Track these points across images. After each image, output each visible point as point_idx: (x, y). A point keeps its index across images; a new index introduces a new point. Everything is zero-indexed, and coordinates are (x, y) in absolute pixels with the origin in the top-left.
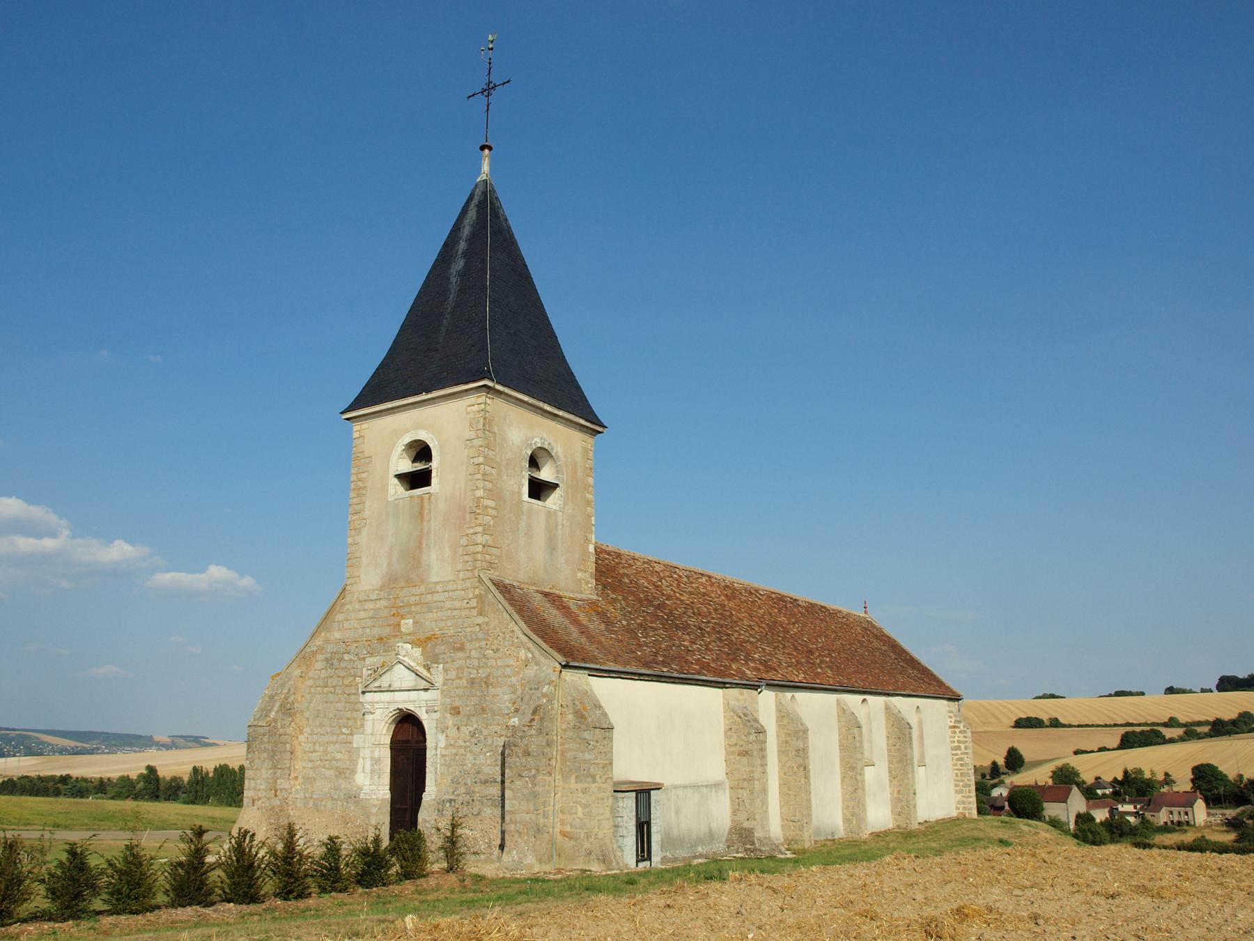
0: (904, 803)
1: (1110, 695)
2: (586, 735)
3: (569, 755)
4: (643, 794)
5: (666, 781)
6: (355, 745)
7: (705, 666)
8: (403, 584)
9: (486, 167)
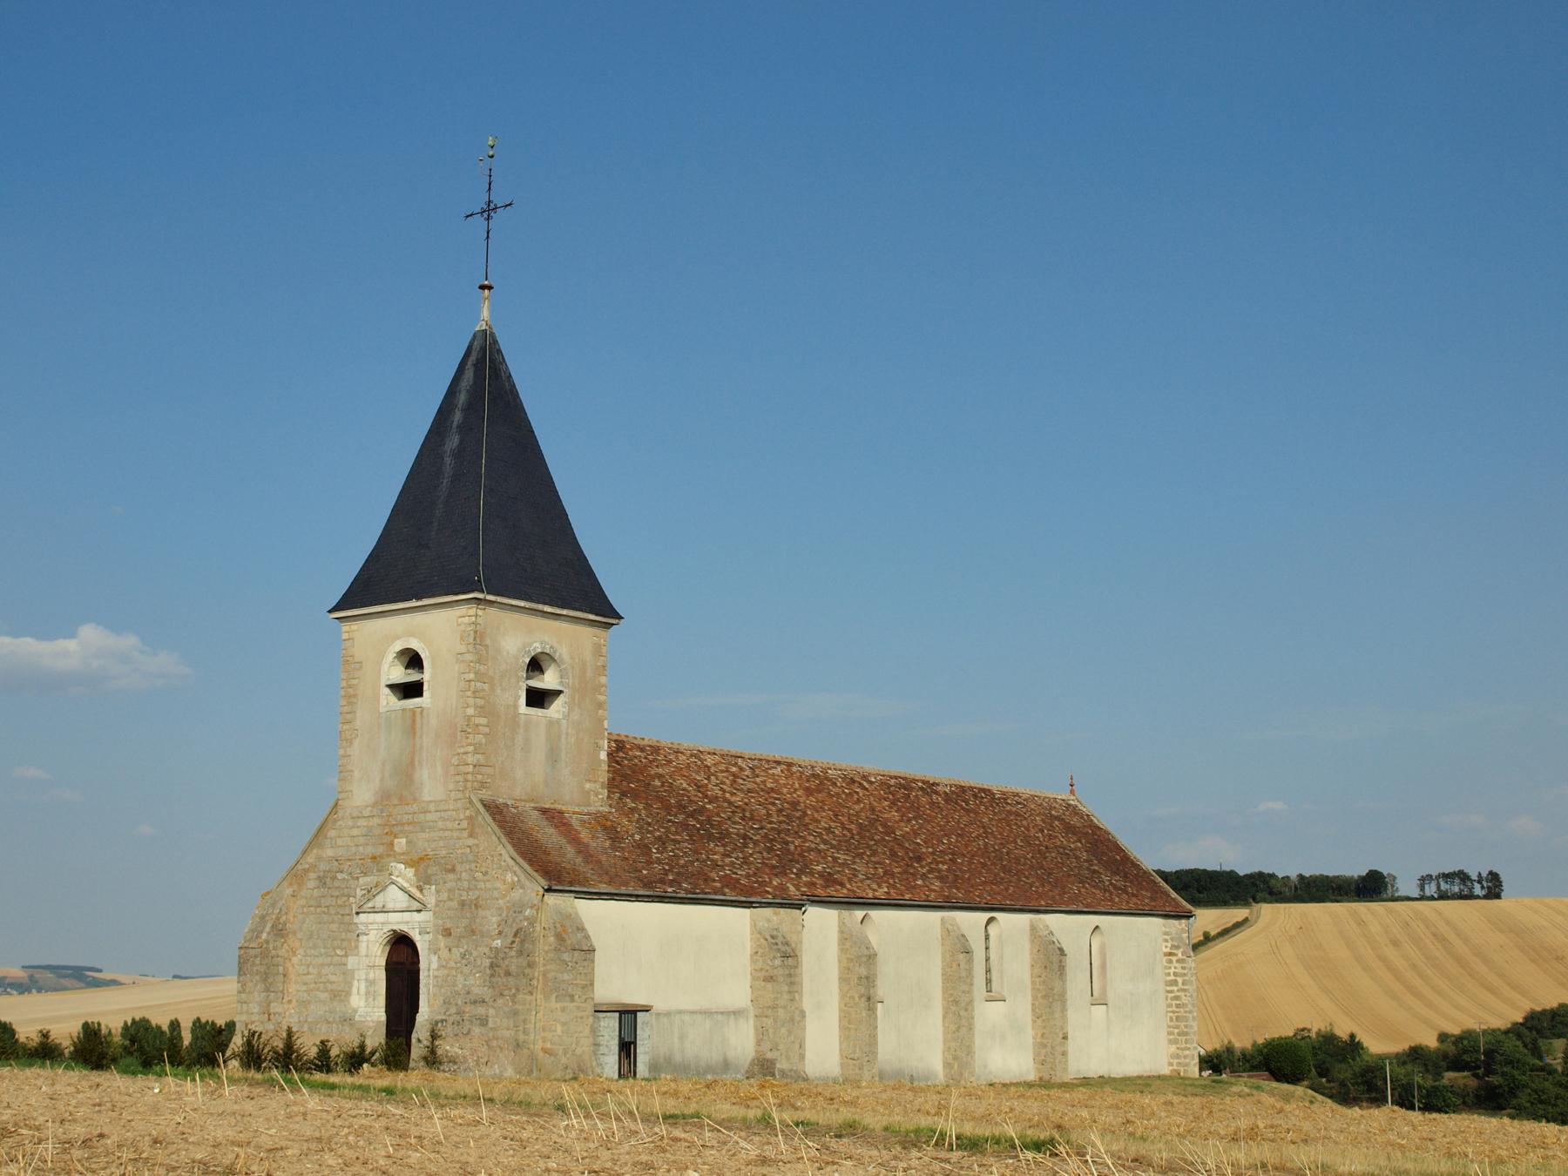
2: (566, 956)
3: (550, 975)
4: (628, 1015)
5: (659, 1005)
7: (730, 883)
9: (485, 314)
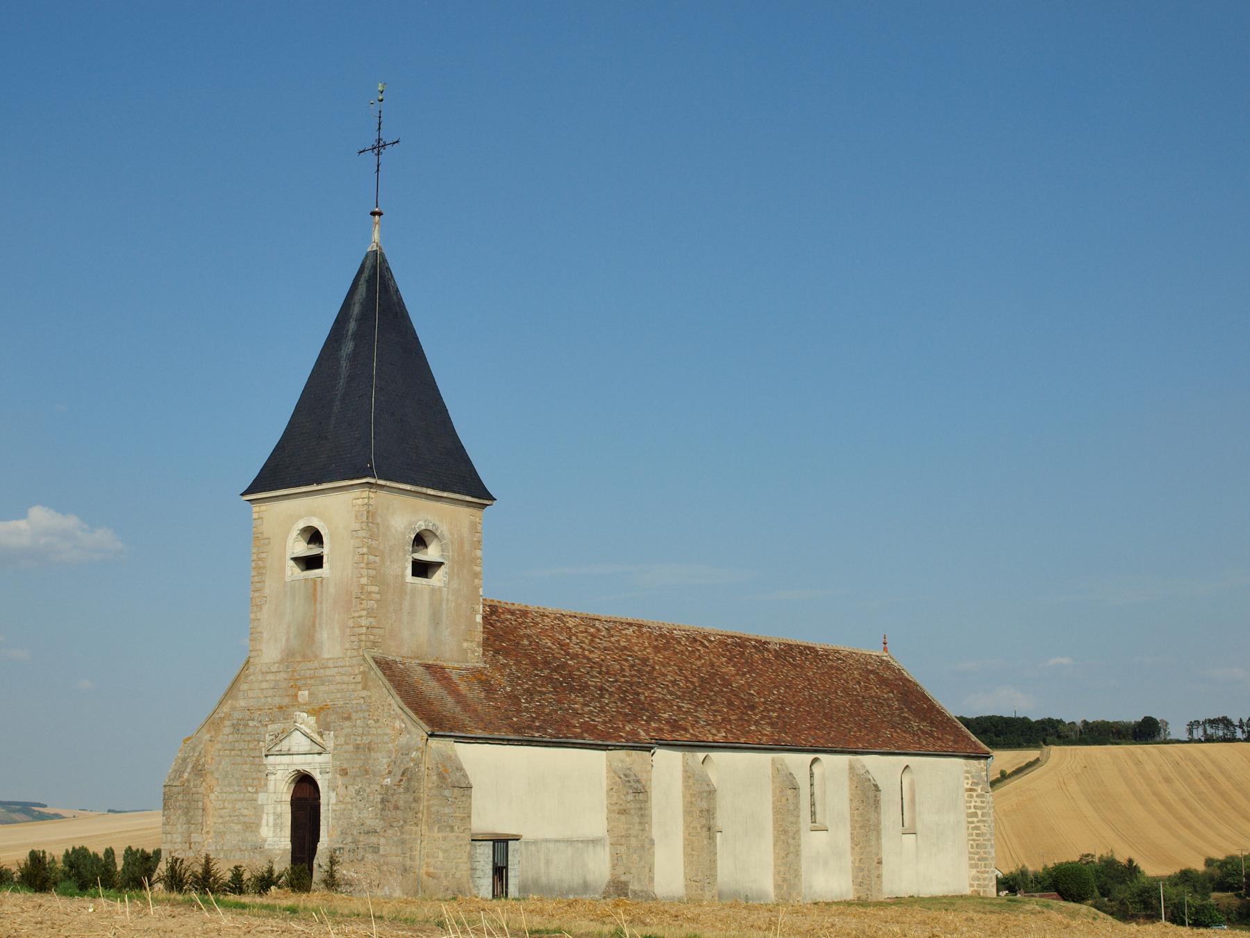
0: (866, 872)
2: (447, 793)
3: (434, 809)
4: (501, 843)
5: (527, 835)
8: (299, 659)
9: (376, 236)
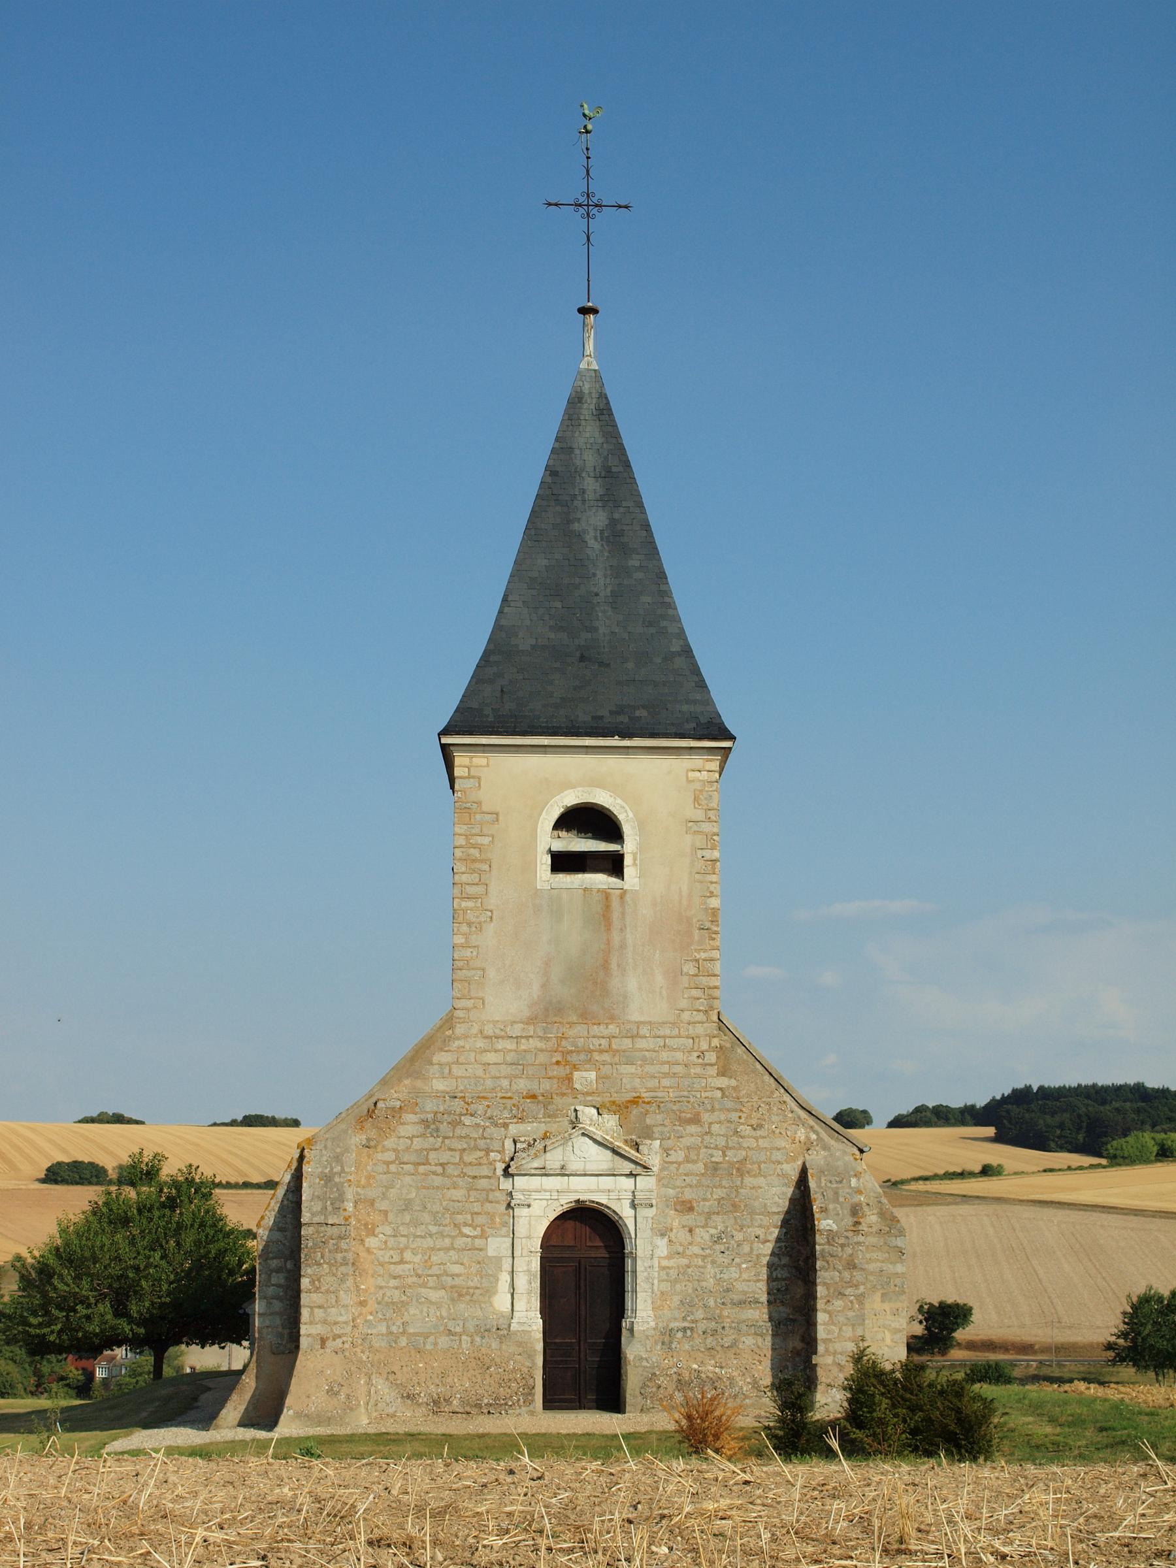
1: (233, 1123)
6: (491, 1253)
